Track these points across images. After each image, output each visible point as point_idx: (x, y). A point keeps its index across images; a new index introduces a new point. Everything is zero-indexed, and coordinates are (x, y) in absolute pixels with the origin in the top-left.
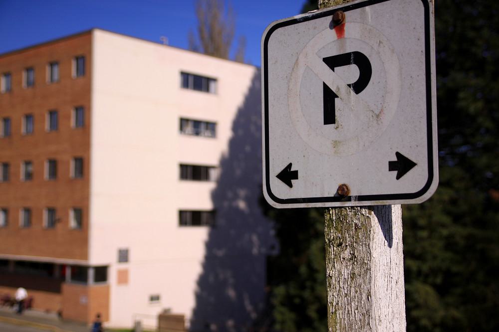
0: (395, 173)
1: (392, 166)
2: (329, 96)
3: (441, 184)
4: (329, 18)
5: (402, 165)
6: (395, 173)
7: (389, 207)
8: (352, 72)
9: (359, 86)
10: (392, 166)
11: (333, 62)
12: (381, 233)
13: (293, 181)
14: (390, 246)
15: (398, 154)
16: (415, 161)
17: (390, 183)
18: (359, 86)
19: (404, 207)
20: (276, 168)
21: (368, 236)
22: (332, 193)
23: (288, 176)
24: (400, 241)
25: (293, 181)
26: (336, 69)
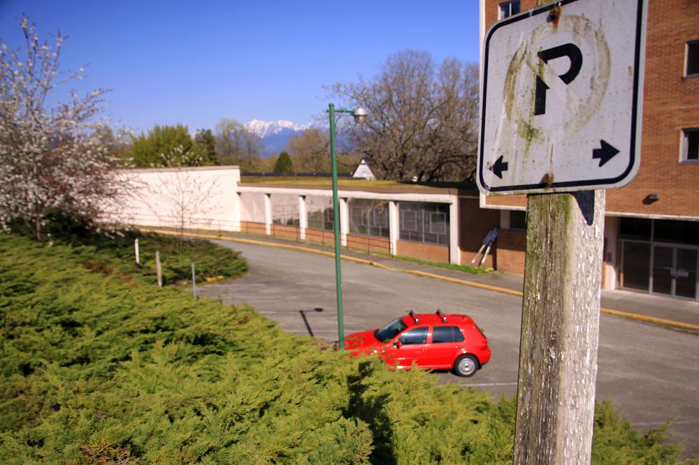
0: (598, 160)
1: (596, 154)
2: (541, 88)
3: (642, 165)
4: (548, 13)
5: (605, 153)
6: (598, 160)
7: (593, 192)
8: (563, 64)
9: (568, 78)
10: (596, 154)
11: (546, 55)
12: (580, 212)
13: (503, 172)
14: (590, 222)
15: (603, 142)
16: (618, 149)
17: (593, 170)
18: (568, 78)
19: (609, 192)
20: (491, 158)
21: (567, 213)
22: (537, 181)
23: (500, 167)
24: (598, 327)
25: (503, 172)
26: (549, 62)
